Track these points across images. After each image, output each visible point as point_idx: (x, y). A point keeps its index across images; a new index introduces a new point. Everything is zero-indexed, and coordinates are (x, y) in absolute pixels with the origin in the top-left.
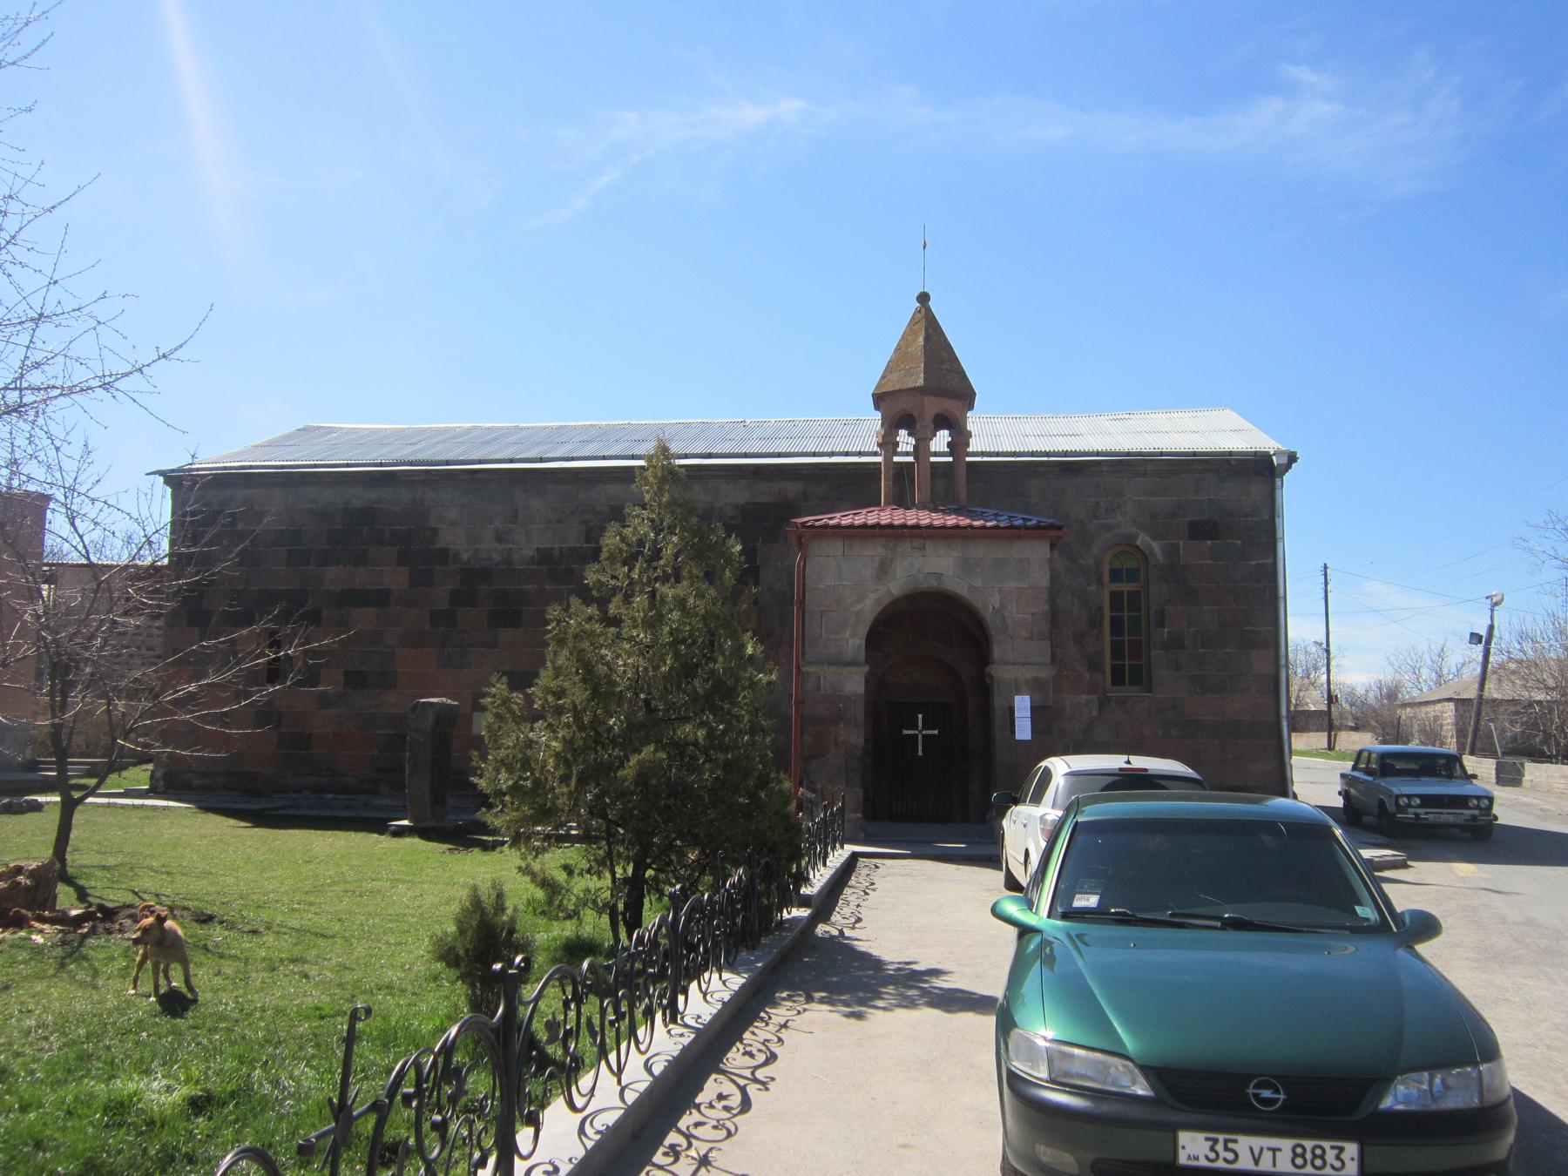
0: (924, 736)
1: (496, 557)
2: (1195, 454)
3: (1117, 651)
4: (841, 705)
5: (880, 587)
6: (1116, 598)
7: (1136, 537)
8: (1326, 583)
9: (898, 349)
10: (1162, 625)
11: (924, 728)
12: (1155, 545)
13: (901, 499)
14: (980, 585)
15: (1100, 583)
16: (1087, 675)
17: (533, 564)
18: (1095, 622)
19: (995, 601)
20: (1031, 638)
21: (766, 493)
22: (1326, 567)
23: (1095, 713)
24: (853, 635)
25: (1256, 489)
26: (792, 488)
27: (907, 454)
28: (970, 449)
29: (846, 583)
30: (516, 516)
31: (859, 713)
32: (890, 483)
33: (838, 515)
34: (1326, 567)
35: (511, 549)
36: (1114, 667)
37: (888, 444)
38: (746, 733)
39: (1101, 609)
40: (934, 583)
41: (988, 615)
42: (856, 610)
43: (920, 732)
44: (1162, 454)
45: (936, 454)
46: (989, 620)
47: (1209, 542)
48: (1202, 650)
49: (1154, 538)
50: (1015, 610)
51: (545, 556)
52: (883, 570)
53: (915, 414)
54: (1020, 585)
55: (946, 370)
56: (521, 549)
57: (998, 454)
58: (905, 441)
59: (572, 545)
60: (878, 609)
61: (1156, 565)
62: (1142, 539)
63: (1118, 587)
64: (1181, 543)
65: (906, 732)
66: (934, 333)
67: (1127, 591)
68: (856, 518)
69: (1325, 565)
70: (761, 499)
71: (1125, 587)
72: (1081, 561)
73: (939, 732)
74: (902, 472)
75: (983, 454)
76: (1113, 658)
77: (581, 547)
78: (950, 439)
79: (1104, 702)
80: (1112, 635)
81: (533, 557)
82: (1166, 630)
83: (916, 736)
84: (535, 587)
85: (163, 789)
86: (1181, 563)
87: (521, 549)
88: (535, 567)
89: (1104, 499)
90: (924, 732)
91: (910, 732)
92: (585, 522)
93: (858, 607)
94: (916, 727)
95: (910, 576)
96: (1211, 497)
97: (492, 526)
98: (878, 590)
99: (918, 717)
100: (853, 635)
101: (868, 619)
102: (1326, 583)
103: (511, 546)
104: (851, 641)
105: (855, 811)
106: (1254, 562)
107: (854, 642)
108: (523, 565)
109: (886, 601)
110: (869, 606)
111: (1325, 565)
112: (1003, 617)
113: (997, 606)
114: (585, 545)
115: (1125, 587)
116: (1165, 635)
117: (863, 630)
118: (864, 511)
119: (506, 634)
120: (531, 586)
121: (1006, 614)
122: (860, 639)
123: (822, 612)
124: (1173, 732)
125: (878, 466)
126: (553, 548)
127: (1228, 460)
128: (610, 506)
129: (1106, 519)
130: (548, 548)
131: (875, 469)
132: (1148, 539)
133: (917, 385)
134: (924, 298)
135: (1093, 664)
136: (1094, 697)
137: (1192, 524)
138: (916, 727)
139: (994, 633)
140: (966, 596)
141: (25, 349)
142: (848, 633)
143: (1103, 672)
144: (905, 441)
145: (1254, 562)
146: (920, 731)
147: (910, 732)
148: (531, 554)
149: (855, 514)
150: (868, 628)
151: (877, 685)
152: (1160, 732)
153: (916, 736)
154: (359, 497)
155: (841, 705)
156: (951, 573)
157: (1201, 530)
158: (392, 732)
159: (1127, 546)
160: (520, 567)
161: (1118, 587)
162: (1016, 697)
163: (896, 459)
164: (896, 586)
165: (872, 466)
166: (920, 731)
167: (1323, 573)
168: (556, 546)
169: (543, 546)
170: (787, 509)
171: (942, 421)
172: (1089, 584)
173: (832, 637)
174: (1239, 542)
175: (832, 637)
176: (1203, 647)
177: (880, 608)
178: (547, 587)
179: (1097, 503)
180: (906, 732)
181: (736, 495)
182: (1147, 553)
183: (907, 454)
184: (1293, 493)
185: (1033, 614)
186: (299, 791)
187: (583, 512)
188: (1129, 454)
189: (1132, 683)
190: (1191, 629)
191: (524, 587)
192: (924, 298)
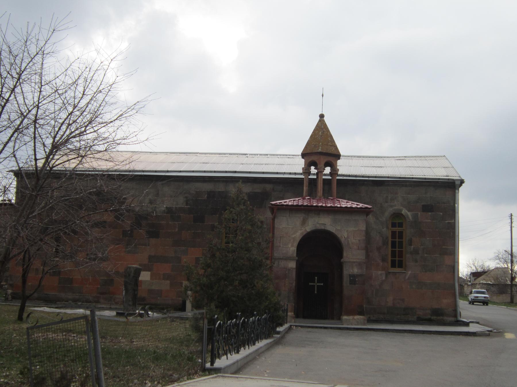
0: (317, 285)
2: (425, 179)
4: (287, 272)
5: (303, 228)
6: (393, 234)
7: (401, 210)
10: (411, 245)
12: (409, 214)
13: (312, 193)
14: (340, 229)
15: (388, 228)
16: (381, 264)
20: (358, 249)
21: (258, 188)
22: (511, 215)
23: (384, 278)
24: (292, 246)
26: (268, 187)
28: (339, 173)
30: (158, 194)
31: (294, 274)
33: (288, 200)
35: (156, 207)
36: (392, 260)
38: (121, 337)
40: (323, 228)
41: (343, 240)
44: (413, 178)
45: (325, 175)
46: (342, 242)
47: (430, 213)
48: (426, 255)
49: (409, 211)
51: (169, 210)
53: (317, 162)
54: (354, 229)
55: (330, 145)
56: (160, 207)
57: (349, 176)
58: (313, 170)
59: (180, 206)
60: (301, 237)
61: (409, 222)
62: (404, 211)
63: (394, 229)
64: (419, 213)
65: (310, 284)
66: (325, 131)
67: (398, 232)
69: (511, 214)
71: (397, 229)
72: (380, 219)
73: (316, 277)
74: (313, 183)
78: (330, 171)
79: (388, 274)
81: (164, 211)
82: (412, 247)
85: (11, 299)
86: (419, 221)
87: (160, 207)
91: (312, 284)
92: (186, 197)
93: (293, 236)
95: (314, 224)
96: (431, 196)
97: (148, 198)
99: (322, 283)
100: (292, 246)
101: (298, 240)
103: (155, 206)
104: (291, 248)
105: (291, 312)
106: (447, 222)
107: (292, 249)
109: (305, 233)
110: (298, 235)
111: (511, 214)
112: (348, 241)
113: (346, 237)
114: (186, 206)
115: (397, 229)
117: (296, 244)
118: (297, 199)
119: (153, 241)
121: (349, 240)
125: (302, 179)
126: (173, 207)
128: (196, 191)
129: (391, 203)
130: (171, 207)
132: (407, 211)
134: (322, 116)
135: (384, 260)
136: (384, 272)
137: (423, 206)
140: (334, 233)
142: (290, 245)
144: (313, 170)
145: (447, 222)
146: (316, 284)
147: (312, 284)
148: (163, 209)
150: (298, 243)
151: (300, 266)
152: (409, 287)
154: (208, 187)
155: (287, 272)
156: (329, 224)
157: (427, 208)
159: (398, 215)
160: (159, 214)
161: (394, 229)
164: (309, 227)
166: (316, 284)
168: (174, 206)
169: (169, 206)
171: (327, 164)
172: (383, 228)
173: (284, 246)
175: (284, 246)
176: (426, 254)
177: (303, 235)
178: (170, 223)
179: (387, 197)
180: (310, 284)
181: (247, 189)
182: (406, 217)
185: (359, 240)
186: (67, 301)
187: (185, 193)
188: (400, 178)
189: (399, 267)
191: (161, 222)
192: (322, 116)
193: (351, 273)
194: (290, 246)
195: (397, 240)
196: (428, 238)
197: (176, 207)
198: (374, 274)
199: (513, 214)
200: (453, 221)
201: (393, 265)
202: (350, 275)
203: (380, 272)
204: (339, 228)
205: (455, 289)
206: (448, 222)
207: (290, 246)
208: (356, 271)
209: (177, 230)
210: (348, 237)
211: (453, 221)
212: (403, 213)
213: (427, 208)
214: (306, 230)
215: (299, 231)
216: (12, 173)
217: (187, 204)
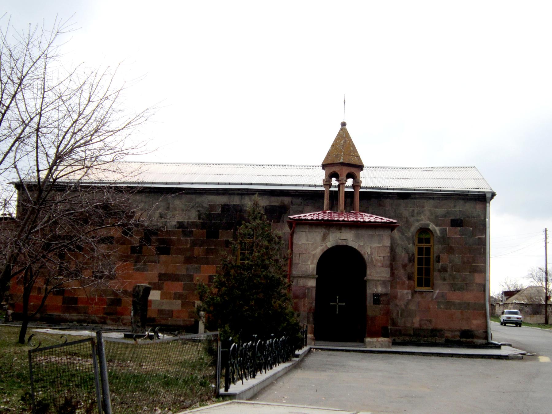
1: (160, 225)
3: (420, 271)
5: (323, 244)
6: (420, 250)
8: (546, 238)
9: (332, 146)
10: (438, 261)
11: (339, 302)
14: (363, 245)
15: (414, 244)
16: (407, 282)
17: (176, 228)
18: (411, 260)
19: (369, 251)
20: (383, 266)
21: (275, 201)
22: (546, 230)
23: (410, 297)
24: (312, 263)
25: (479, 206)
26: (287, 200)
27: (335, 187)
29: (309, 242)
30: (169, 207)
32: (328, 201)
34: (546, 230)
35: (166, 221)
37: (327, 184)
39: (413, 254)
40: (344, 243)
41: (366, 257)
42: (313, 253)
43: (338, 304)
45: (347, 187)
47: (459, 228)
48: (455, 273)
49: (437, 225)
50: (376, 255)
51: (181, 225)
52: (324, 238)
56: (171, 222)
57: (373, 188)
58: (334, 182)
59: (192, 221)
60: (321, 253)
61: (437, 237)
62: (432, 226)
63: (421, 245)
64: (448, 228)
65: (331, 304)
68: (314, 216)
69: (546, 229)
70: (273, 204)
71: (424, 245)
72: (406, 234)
74: (334, 196)
75: (367, 188)
76: (418, 275)
77: (196, 222)
79: (414, 293)
80: (418, 265)
81: (175, 225)
82: (440, 264)
83: (336, 305)
84: (176, 238)
87: (171, 222)
88: (176, 229)
89: (416, 209)
90: (339, 304)
92: (199, 211)
93: (313, 253)
94: (336, 302)
98: (322, 245)
100: (312, 263)
102: (546, 238)
103: (165, 220)
105: (311, 334)
106: (477, 237)
107: (311, 267)
108: (171, 228)
109: (325, 250)
110: (319, 252)
111: (546, 229)
113: (369, 253)
114: (198, 221)
115: (424, 245)
116: (440, 266)
117: (316, 261)
118: (317, 213)
119: (163, 258)
120: (174, 238)
121: (373, 256)
122: (315, 265)
123: (299, 254)
124: (442, 306)
125: (323, 192)
126: (184, 222)
127: (467, 195)
130: (182, 222)
131: (322, 193)
132: (434, 226)
133: (340, 162)
134: (344, 124)
135: (410, 278)
136: (410, 291)
137: (452, 220)
138: (336, 302)
139: (368, 264)
141: (40, 169)
143: (414, 281)
144: (334, 182)
145: (477, 237)
149: (314, 214)
153: (336, 305)
154: (222, 200)
157: (456, 223)
158: (113, 298)
161: (421, 245)
162: (181, 301)
163: (331, 189)
165: (320, 192)
167: (545, 233)
168: (186, 221)
170: (283, 210)
171: (349, 176)
174: (471, 228)
176: (455, 272)
178: (182, 238)
179: (413, 210)
182: (433, 232)
183: (335, 187)
184: (493, 207)
185: (383, 257)
187: (197, 207)
188: (427, 190)
190: (450, 264)
191: (172, 238)
192: (344, 124)
193: (375, 293)
194: (309, 263)
195: (424, 257)
196: (457, 255)
197: (188, 222)
198: (399, 294)
199: (547, 229)
200: (484, 237)
201: (420, 284)
202: (373, 294)
203: (406, 291)
204: (362, 244)
205: (485, 310)
206: (478, 238)
207: (309, 263)
208: (380, 290)
209: (189, 246)
210: (372, 254)
211: (484, 237)
212: (430, 227)
213: (456, 223)
214: (326, 246)
215: (320, 247)
216: (13, 186)
217: (199, 219)
